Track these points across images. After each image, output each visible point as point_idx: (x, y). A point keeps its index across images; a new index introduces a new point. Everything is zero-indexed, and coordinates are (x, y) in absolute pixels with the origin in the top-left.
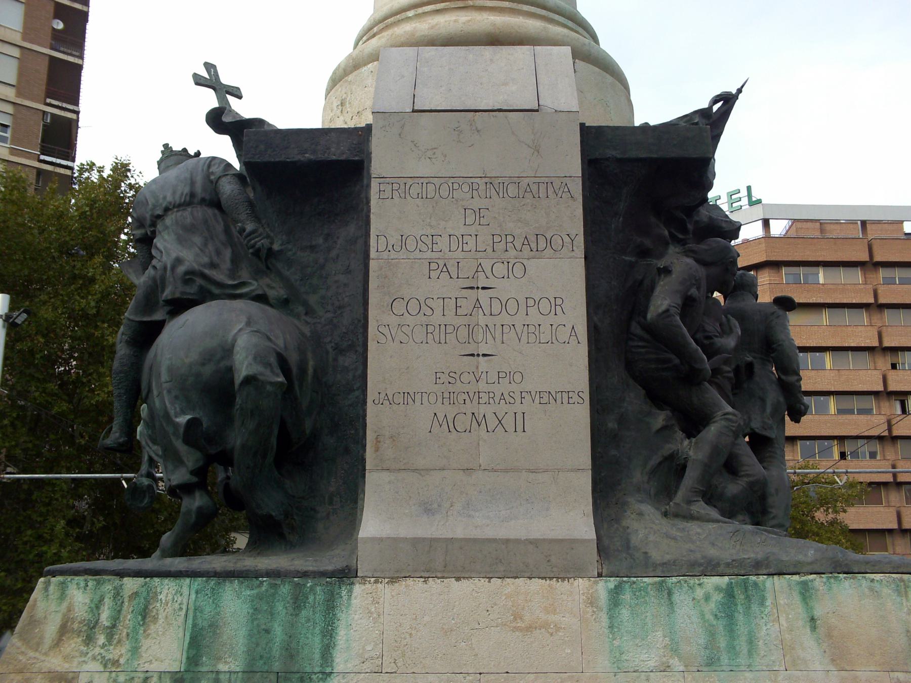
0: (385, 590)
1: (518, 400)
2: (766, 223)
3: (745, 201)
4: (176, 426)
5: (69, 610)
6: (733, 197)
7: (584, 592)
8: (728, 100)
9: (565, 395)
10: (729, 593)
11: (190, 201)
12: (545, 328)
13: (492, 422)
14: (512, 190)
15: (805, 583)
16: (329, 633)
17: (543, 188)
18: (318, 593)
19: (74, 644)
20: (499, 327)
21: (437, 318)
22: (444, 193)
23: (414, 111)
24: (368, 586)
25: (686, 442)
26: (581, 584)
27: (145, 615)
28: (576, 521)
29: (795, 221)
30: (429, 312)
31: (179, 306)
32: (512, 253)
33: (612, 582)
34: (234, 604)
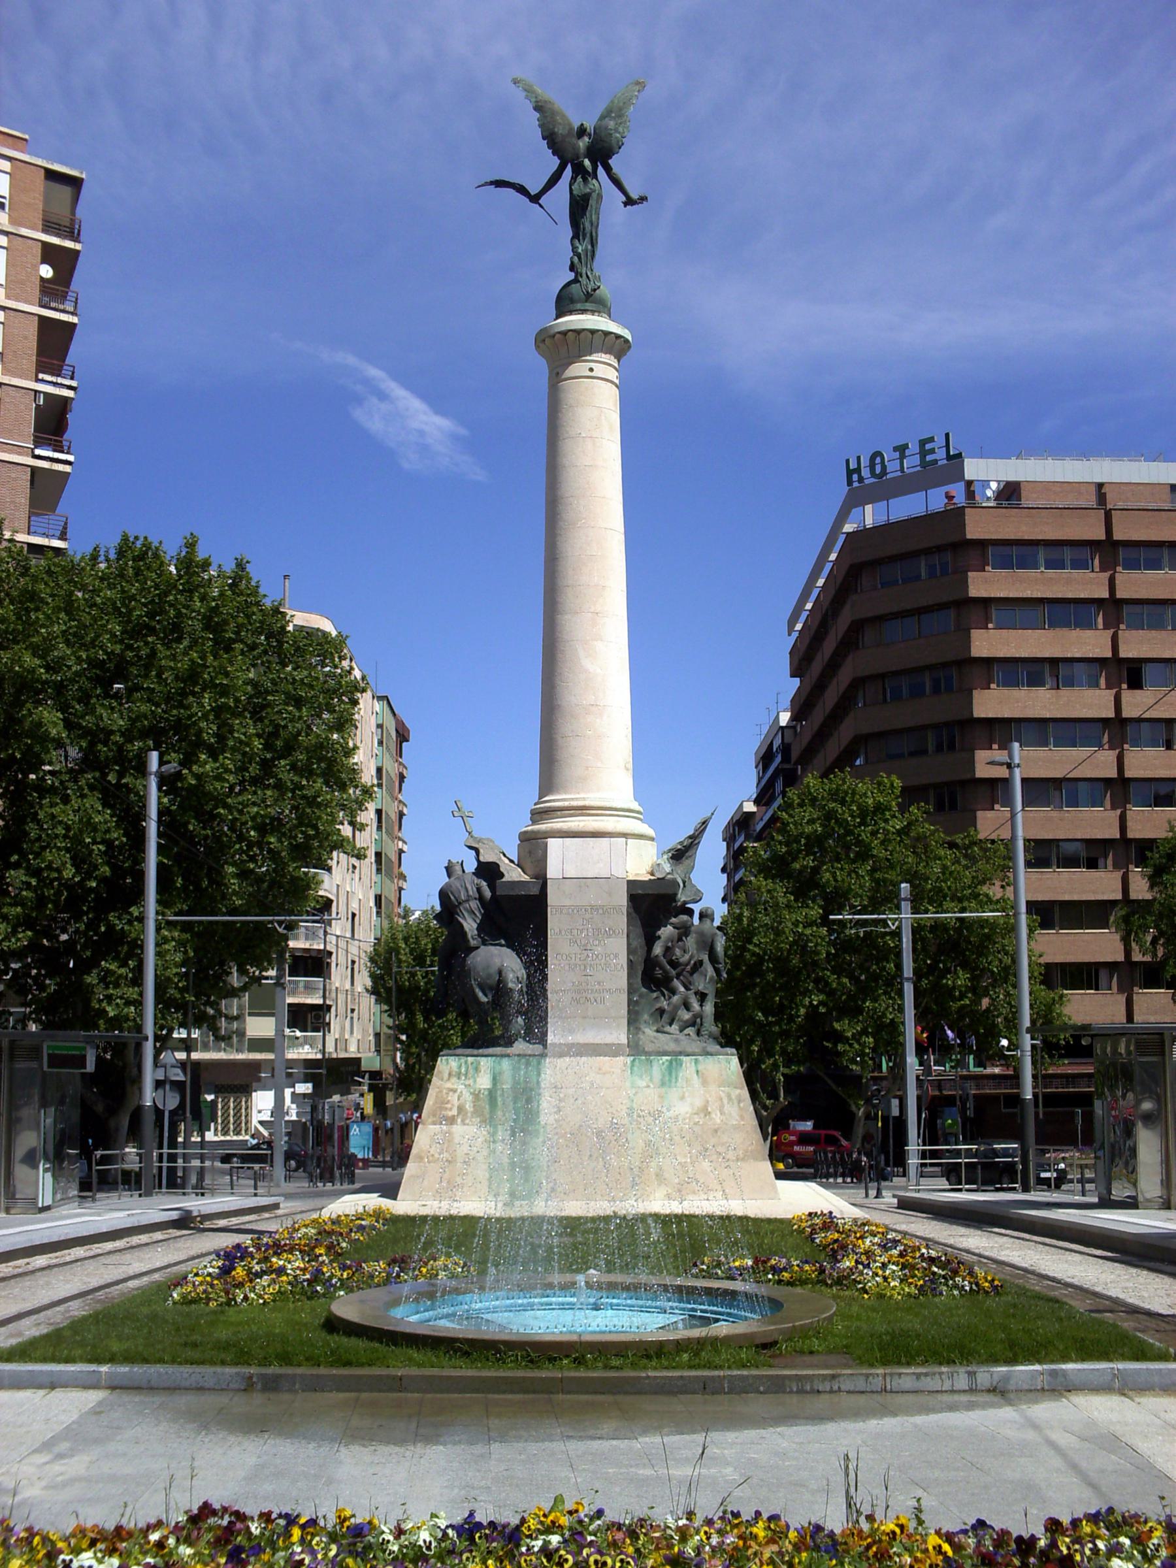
6: (928, 447)
7: (623, 1061)
8: (705, 823)
10: (671, 1062)
14: (601, 911)
19: (454, 1080)
27: (477, 1070)
28: (619, 1035)
34: (506, 1064)
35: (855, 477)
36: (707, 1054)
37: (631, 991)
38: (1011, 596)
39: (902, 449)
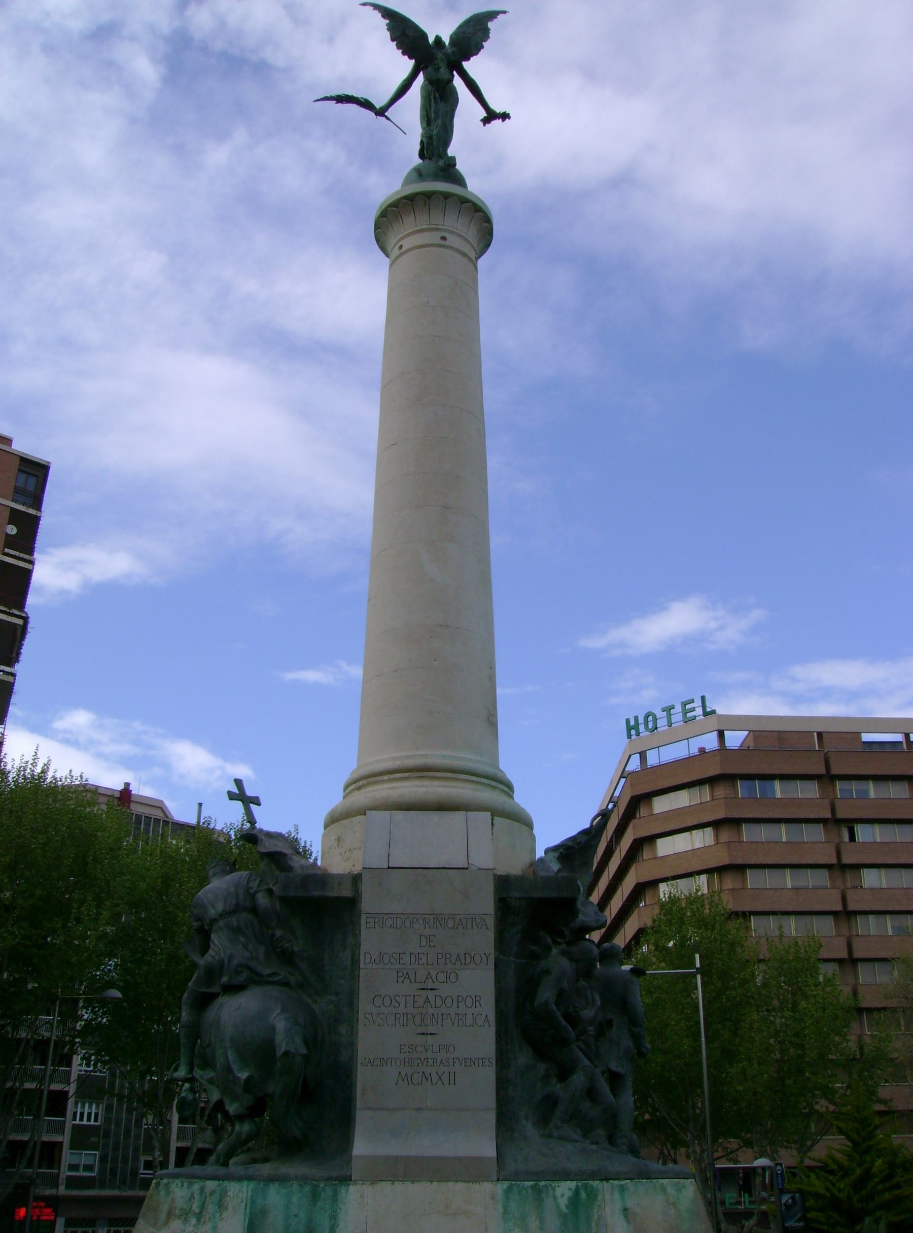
0: (368, 1189)
1: (452, 1063)
2: (721, 734)
3: (699, 711)
4: (236, 1080)
5: (173, 1201)
6: (688, 707)
9: (481, 1061)
11: (235, 910)
12: (470, 1017)
13: (435, 1078)
14: (450, 924)
15: (622, 1186)
16: (334, 1217)
17: (469, 922)
18: (327, 1192)
20: (440, 1015)
21: (401, 1009)
22: (408, 924)
23: (389, 868)
24: (358, 1186)
25: (558, 1086)
26: (487, 1186)
27: (221, 1206)
29: (750, 731)
30: (397, 1005)
31: (233, 989)
32: (449, 965)
33: (505, 1185)
35: (633, 732)
36: (646, 1175)
37: (503, 1059)
38: (757, 816)
39: (668, 710)
